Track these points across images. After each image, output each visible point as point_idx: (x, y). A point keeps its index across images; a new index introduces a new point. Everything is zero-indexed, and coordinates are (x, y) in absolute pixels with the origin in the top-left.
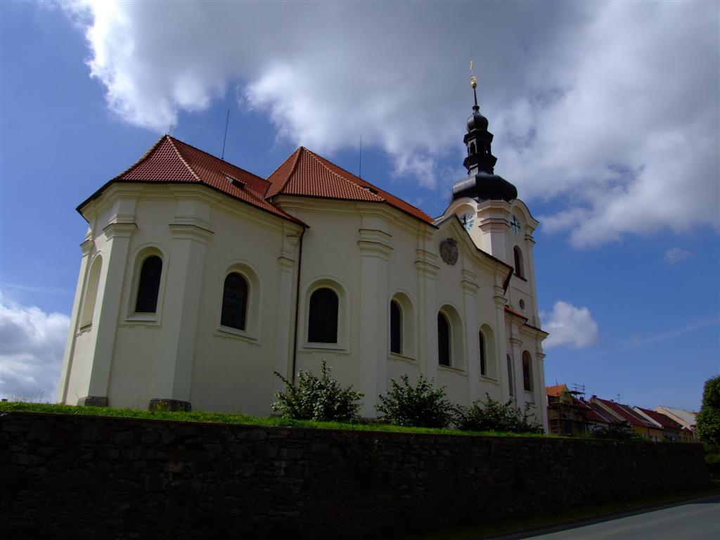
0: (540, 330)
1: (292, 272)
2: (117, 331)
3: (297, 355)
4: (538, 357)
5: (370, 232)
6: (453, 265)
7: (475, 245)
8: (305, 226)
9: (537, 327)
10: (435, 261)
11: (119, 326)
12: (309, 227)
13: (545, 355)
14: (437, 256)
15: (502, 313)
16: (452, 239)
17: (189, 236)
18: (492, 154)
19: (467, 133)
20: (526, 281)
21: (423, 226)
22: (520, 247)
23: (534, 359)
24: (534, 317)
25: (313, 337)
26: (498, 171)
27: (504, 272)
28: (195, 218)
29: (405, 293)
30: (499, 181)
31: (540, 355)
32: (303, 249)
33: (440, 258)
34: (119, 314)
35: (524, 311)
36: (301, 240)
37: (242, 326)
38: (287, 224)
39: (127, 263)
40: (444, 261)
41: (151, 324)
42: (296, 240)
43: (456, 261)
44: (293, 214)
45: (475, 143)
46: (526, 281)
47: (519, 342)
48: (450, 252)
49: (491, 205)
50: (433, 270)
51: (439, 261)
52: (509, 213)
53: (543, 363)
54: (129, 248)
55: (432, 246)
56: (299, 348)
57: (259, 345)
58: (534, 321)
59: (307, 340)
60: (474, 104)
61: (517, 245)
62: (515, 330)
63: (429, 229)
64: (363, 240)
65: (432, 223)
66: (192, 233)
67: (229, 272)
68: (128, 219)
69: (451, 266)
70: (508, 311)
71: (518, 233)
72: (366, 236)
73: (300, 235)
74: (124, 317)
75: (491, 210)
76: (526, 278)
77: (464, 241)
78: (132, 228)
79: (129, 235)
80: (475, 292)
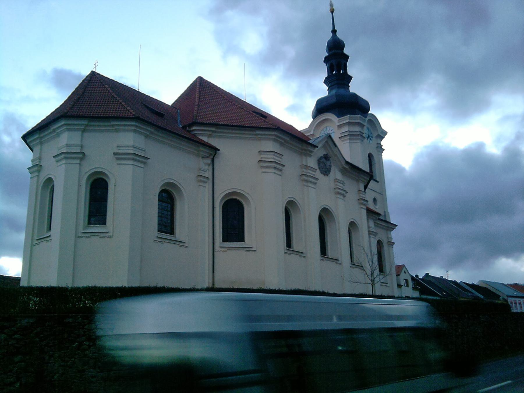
0: (389, 223)
1: (209, 186)
2: (75, 241)
3: (215, 253)
4: (389, 245)
5: (268, 153)
6: (327, 175)
7: (343, 158)
8: (216, 150)
9: (387, 220)
10: (280, 160)
11: (77, 237)
12: (219, 150)
13: (394, 243)
14: (316, 170)
15: (364, 212)
16: (327, 154)
17: (131, 162)
18: (348, 73)
19: (327, 54)
20: (378, 182)
21: (305, 147)
22: (373, 154)
23: (386, 247)
24: (385, 212)
25: (226, 238)
26: (354, 88)
27: (365, 179)
28: (134, 147)
29: (328, 208)
30: (355, 96)
31: (391, 244)
32: (215, 167)
33: (318, 171)
34: (76, 229)
35: (377, 207)
36: (213, 161)
37: (241, 238)
38: (202, 149)
39: (79, 185)
40: (322, 173)
41: (104, 235)
42: (209, 161)
43: (330, 171)
44: (205, 139)
45: (334, 64)
46: (378, 182)
47: (375, 234)
48: (325, 165)
49: (349, 119)
50: (314, 180)
51: (318, 174)
52: (364, 126)
53: (393, 250)
54: (80, 172)
55: (312, 162)
56: (217, 247)
57: (186, 247)
58: (385, 215)
59: (221, 241)
60: (331, 29)
61: (371, 152)
62: (372, 224)
63: (310, 148)
64: (263, 160)
65: (310, 141)
66: (134, 160)
67: (161, 190)
68: (76, 148)
69: (326, 176)
70: (369, 211)
71: (371, 142)
72: (265, 156)
73: (212, 157)
74: (81, 230)
75: (349, 124)
76: (378, 180)
77: (336, 155)
78: (81, 156)
79: (78, 161)
80: (344, 196)
